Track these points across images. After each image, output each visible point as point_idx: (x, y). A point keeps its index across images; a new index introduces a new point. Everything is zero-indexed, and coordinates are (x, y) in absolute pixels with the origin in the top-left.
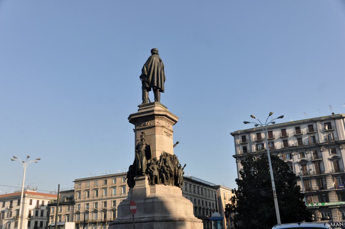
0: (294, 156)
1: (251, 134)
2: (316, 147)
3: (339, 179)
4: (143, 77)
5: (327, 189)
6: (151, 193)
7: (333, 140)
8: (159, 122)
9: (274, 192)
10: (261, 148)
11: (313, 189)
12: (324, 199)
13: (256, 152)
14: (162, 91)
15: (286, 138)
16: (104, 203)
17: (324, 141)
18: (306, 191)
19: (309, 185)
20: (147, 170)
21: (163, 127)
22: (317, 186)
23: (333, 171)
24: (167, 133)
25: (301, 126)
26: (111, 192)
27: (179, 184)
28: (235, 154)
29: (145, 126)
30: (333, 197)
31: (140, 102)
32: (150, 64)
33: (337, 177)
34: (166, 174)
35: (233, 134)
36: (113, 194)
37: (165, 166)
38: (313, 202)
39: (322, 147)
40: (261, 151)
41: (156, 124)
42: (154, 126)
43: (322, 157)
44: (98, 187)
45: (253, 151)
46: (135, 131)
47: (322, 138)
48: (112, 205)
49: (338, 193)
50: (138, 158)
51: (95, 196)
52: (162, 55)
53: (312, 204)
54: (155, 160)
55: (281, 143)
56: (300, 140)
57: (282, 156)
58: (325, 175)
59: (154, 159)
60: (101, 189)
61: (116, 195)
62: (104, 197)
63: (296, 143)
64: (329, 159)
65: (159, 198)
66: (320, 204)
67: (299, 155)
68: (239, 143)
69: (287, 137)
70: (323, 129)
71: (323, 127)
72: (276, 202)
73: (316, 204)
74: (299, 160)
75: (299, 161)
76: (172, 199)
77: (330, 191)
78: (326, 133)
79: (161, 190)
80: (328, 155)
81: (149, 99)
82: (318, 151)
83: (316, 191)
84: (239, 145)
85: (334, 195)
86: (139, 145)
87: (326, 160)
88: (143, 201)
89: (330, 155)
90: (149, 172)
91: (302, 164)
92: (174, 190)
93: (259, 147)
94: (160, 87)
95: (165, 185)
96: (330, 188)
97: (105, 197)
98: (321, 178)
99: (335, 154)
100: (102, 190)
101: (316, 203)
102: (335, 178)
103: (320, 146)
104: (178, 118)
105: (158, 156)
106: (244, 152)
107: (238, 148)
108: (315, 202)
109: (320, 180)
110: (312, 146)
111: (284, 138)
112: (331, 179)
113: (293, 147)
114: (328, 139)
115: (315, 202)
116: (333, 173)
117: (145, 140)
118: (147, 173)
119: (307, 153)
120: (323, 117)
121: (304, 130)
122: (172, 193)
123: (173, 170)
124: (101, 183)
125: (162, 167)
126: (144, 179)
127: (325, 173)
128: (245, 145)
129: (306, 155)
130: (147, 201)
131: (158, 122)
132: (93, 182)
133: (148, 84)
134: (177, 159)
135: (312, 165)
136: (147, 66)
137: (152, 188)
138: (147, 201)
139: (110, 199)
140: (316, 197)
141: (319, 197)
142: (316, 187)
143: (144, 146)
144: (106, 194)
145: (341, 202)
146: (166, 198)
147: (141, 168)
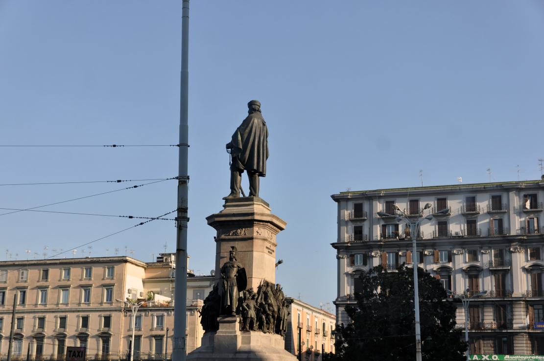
0: (456, 256)
1: (374, 202)
2: (503, 243)
3: (538, 309)
4: (232, 147)
5: (512, 328)
6: (242, 343)
7: (536, 232)
8: (259, 231)
9: (417, 342)
10: (392, 233)
11: (487, 326)
12: (505, 348)
13: (380, 241)
14: (262, 174)
15: (445, 218)
16: (37, 319)
17: (519, 232)
18: (472, 328)
19: (478, 317)
20: (238, 308)
21: (265, 240)
22: (494, 320)
23: (528, 294)
24: (269, 249)
25: (479, 196)
26: (57, 298)
27: (281, 331)
28: (336, 242)
29: (236, 235)
30: (522, 345)
31: (227, 192)
32: (247, 131)
33: (536, 307)
34: (267, 316)
35: (336, 198)
36: (61, 302)
37: (266, 304)
38: (482, 352)
39: (514, 244)
40: (390, 240)
41: (255, 234)
42: (252, 238)
43: (510, 264)
44: (26, 285)
45: (374, 239)
46: (218, 240)
47: (516, 225)
48: (56, 327)
49: (532, 336)
50: (226, 288)
51: (18, 303)
52: (266, 113)
53: (479, 354)
54: (250, 291)
55: (433, 227)
56: (471, 224)
57: (433, 255)
58: (512, 301)
59: (248, 291)
60: (33, 289)
61: (67, 304)
62: (40, 307)
63: (465, 230)
64: (524, 269)
65: (257, 353)
66: (495, 357)
67: (467, 255)
68: (346, 218)
69: (448, 215)
70: (520, 206)
71: (521, 203)
72: (419, 358)
73: (488, 357)
74: (465, 266)
75: (464, 268)
76: (275, 355)
77: (517, 334)
78: (525, 215)
79: (258, 340)
80: (524, 260)
81: (241, 188)
82: (504, 251)
83: (490, 331)
84: (347, 222)
85: (525, 342)
86: (227, 267)
87: (519, 269)
88: (231, 356)
89: (527, 261)
90: (243, 312)
91: (471, 273)
92: (275, 340)
93: (389, 230)
94: (261, 170)
95: (265, 333)
96: (519, 327)
97: (42, 307)
98: (504, 305)
99: (537, 259)
100: (36, 291)
101: (489, 354)
102: (530, 308)
103: (510, 240)
104: (285, 224)
105: (255, 285)
106: (355, 239)
107: (344, 229)
108: (486, 352)
109: (502, 309)
110: (495, 239)
111: (442, 217)
112: (522, 310)
113: (457, 237)
114: (527, 228)
115: (486, 352)
116: (528, 296)
117: (236, 260)
118: (238, 312)
119: (483, 253)
120: (522, 182)
121: (483, 205)
122: (273, 346)
123: (276, 309)
124: (34, 275)
125: (261, 304)
126: (235, 321)
127: (513, 296)
128: (359, 224)
129: (479, 257)
130: (238, 356)
131: (259, 231)
132: (16, 272)
133: (243, 163)
134: (282, 292)
135: (489, 278)
136: (244, 134)
137: (244, 335)
138: (238, 356)
139: (53, 312)
140: (489, 342)
141: (494, 343)
142: (491, 323)
143: (235, 269)
144: (45, 301)
145: (536, 355)
146: (267, 354)
147: (229, 304)
